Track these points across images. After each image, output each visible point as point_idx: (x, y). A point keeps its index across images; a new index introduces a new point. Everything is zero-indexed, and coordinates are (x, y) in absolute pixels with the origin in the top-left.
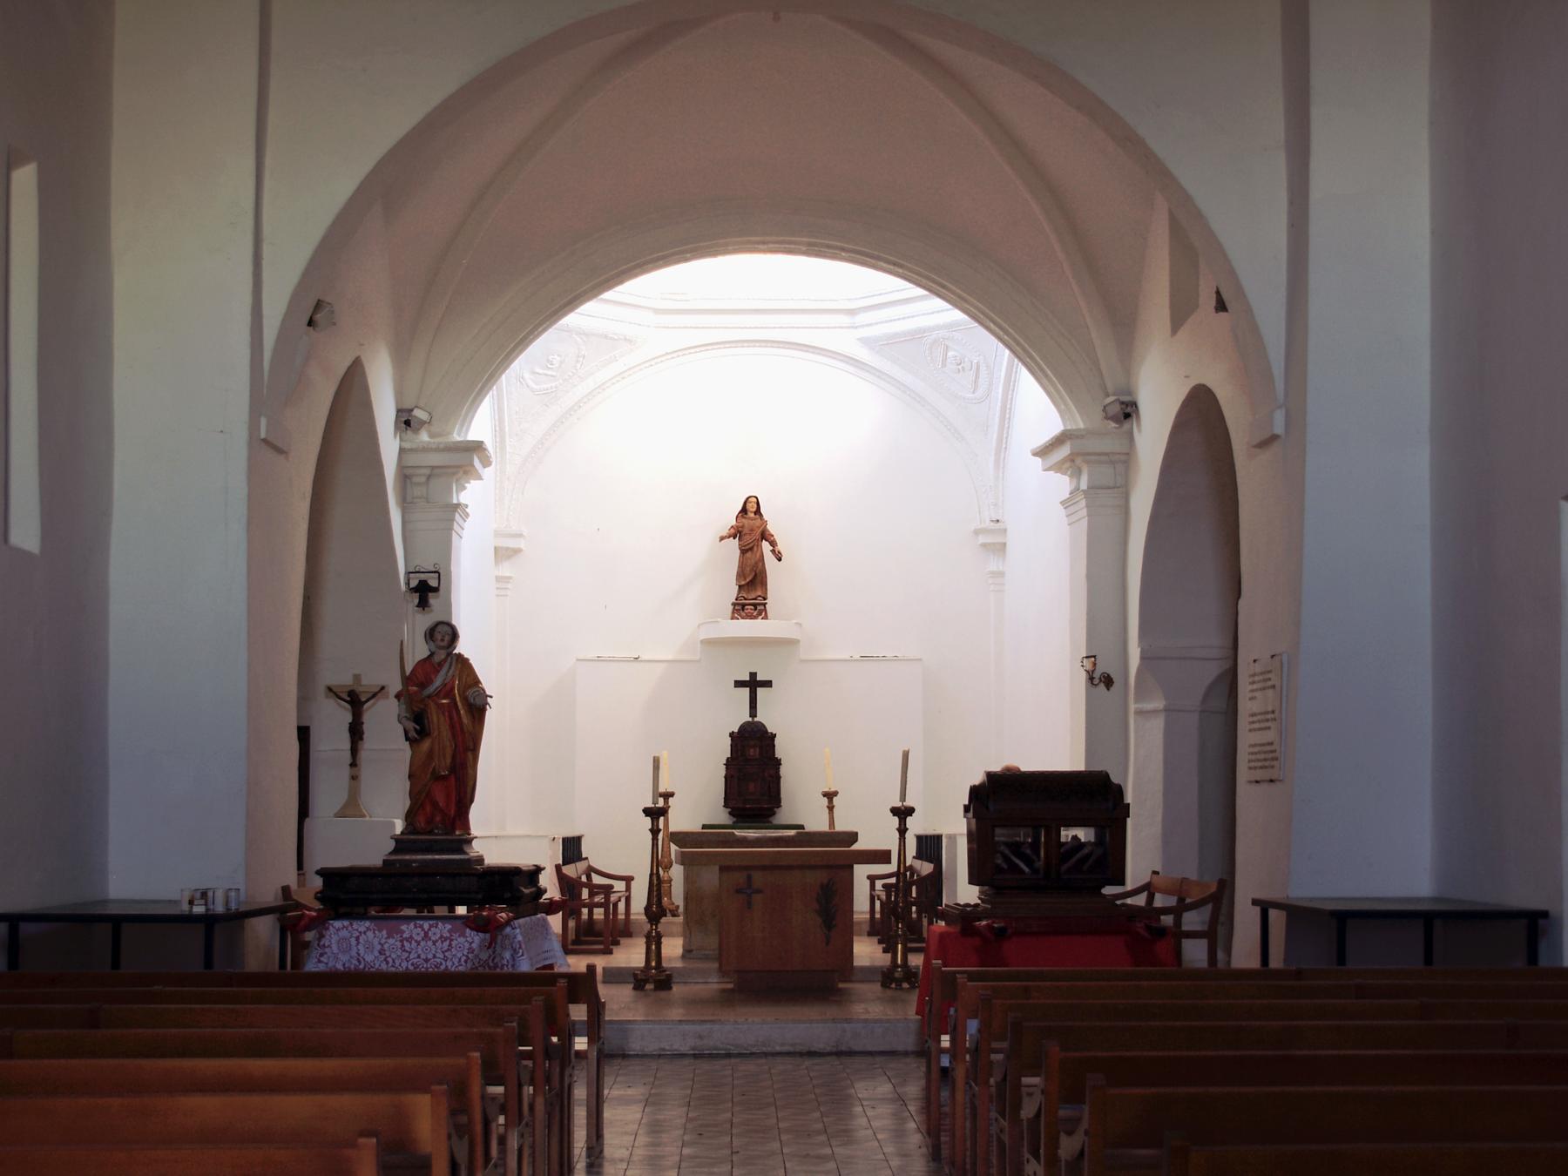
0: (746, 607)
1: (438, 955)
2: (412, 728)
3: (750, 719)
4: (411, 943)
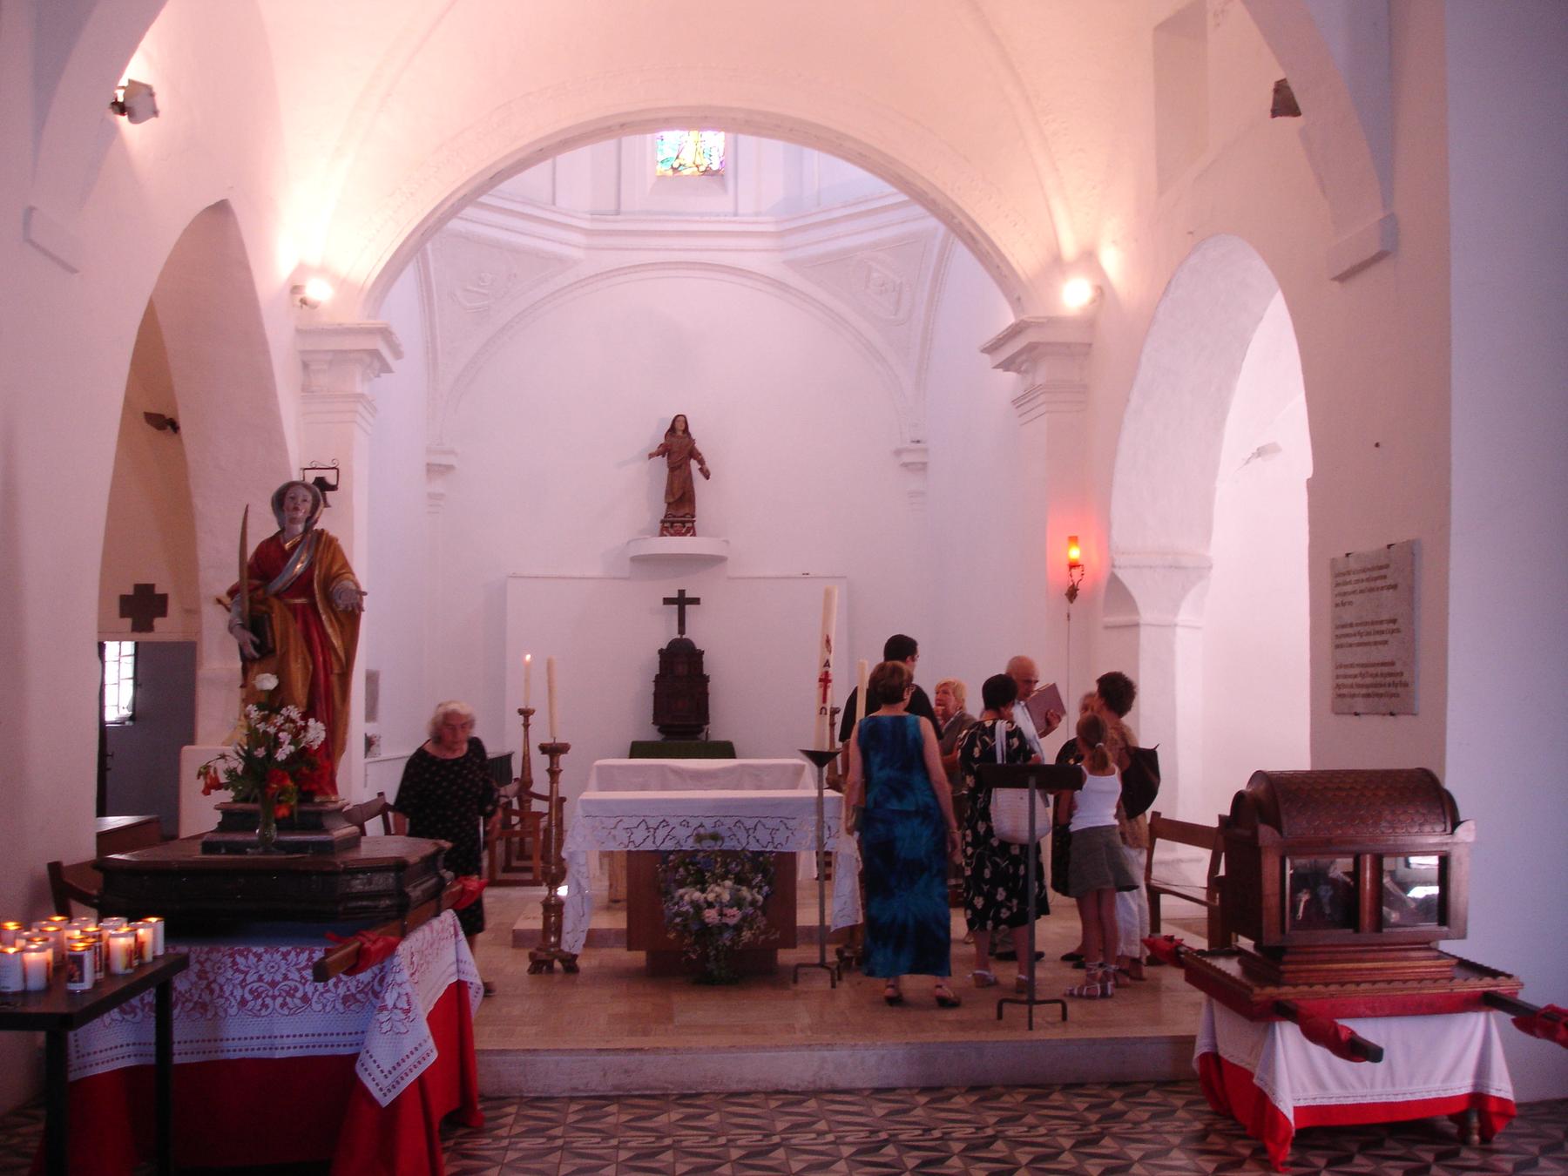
0: (675, 525)
1: (290, 976)
2: (249, 641)
3: (679, 637)
4: (246, 958)
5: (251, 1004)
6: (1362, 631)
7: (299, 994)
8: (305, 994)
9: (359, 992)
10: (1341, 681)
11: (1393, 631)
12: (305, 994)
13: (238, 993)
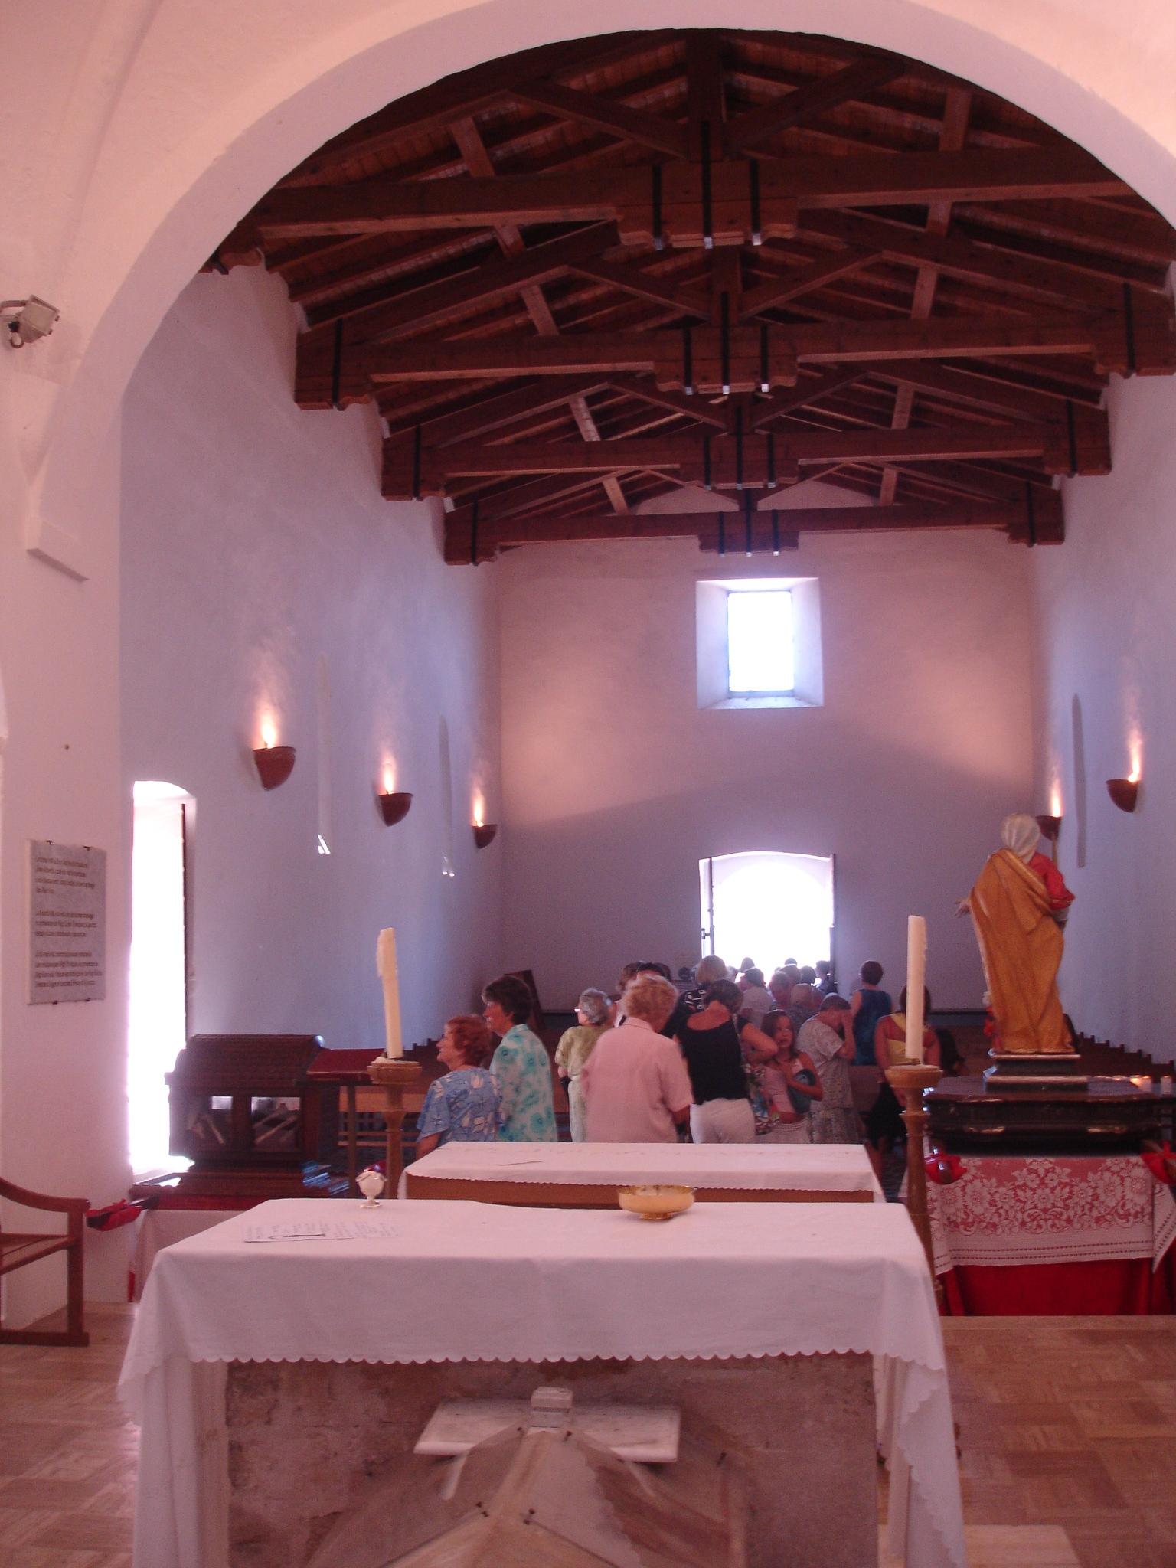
1: (1057, 1204)
5: (1029, 1224)
6: (63, 921)
7: (1064, 1217)
8: (1068, 1217)
9: (1108, 1214)
10: (41, 970)
11: (90, 926)
12: (1068, 1217)
13: (1020, 1216)
